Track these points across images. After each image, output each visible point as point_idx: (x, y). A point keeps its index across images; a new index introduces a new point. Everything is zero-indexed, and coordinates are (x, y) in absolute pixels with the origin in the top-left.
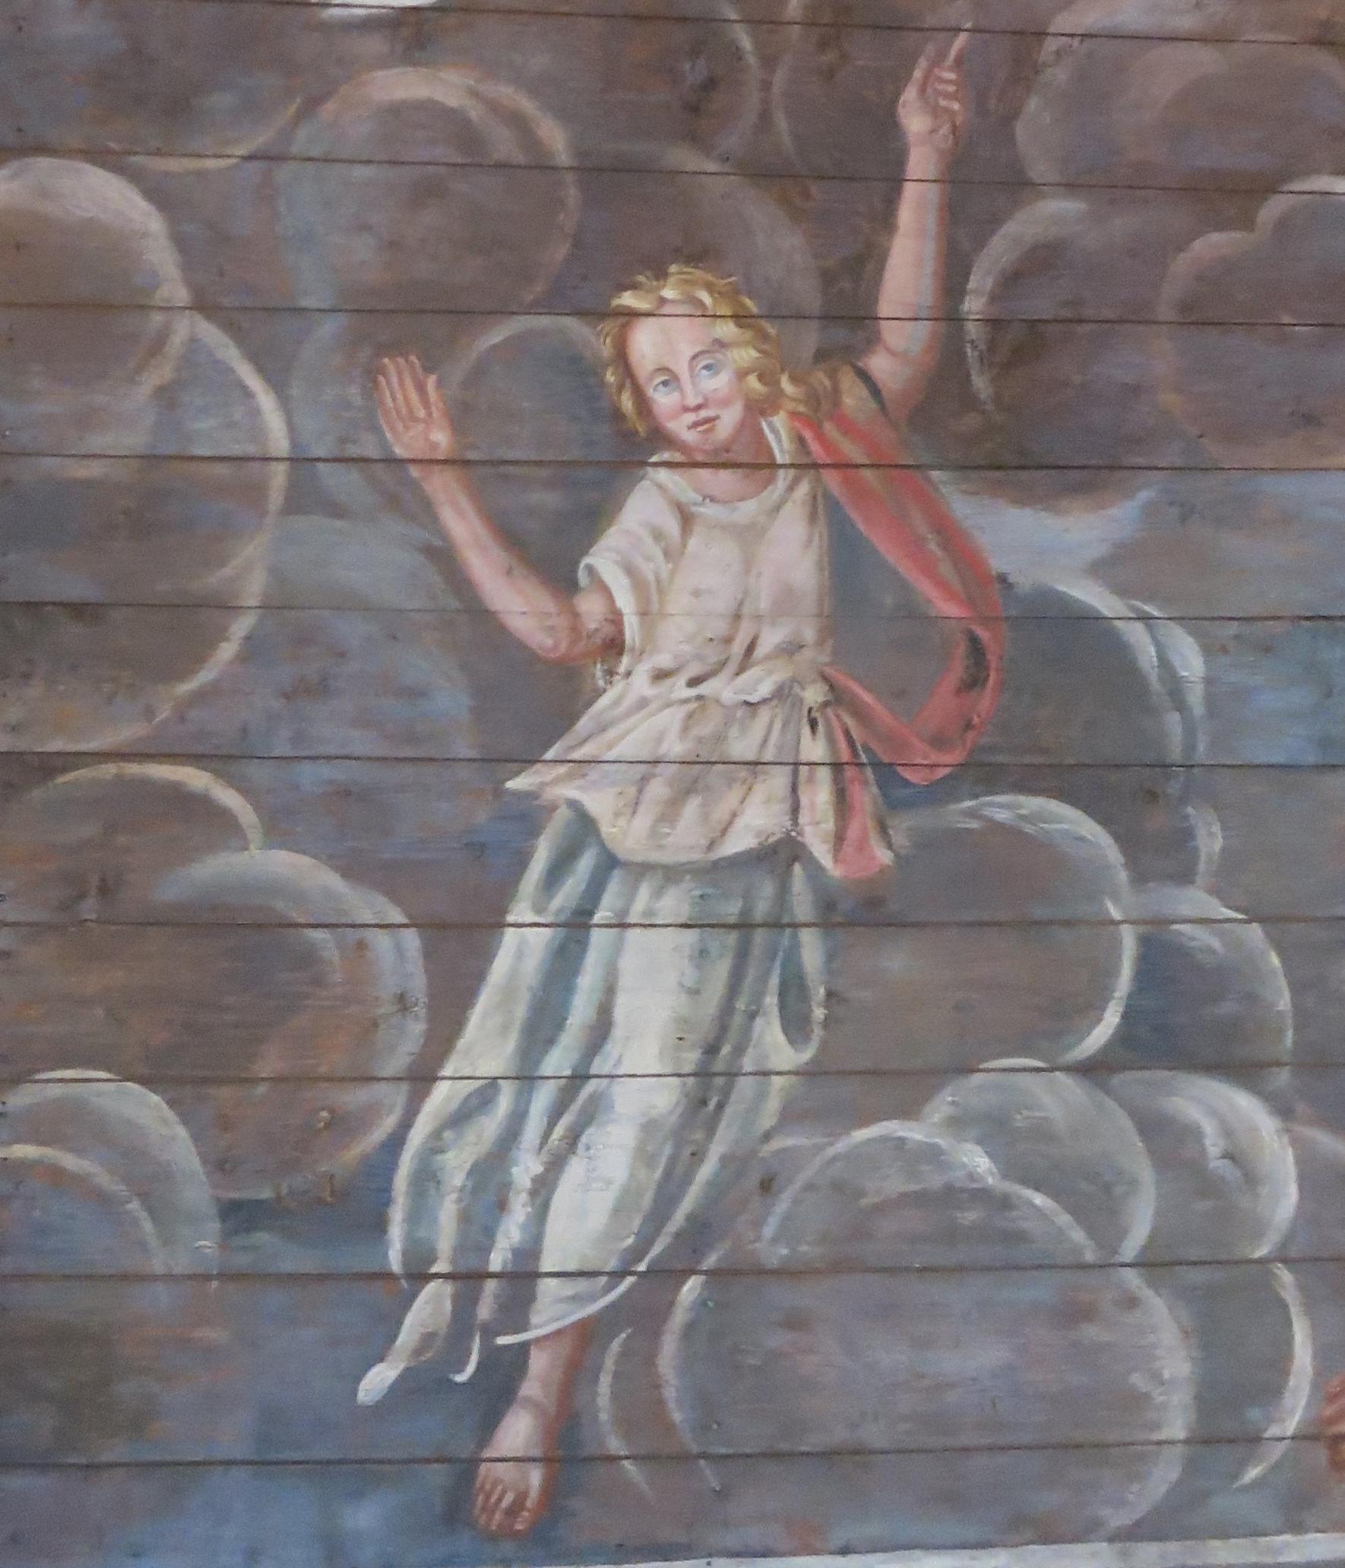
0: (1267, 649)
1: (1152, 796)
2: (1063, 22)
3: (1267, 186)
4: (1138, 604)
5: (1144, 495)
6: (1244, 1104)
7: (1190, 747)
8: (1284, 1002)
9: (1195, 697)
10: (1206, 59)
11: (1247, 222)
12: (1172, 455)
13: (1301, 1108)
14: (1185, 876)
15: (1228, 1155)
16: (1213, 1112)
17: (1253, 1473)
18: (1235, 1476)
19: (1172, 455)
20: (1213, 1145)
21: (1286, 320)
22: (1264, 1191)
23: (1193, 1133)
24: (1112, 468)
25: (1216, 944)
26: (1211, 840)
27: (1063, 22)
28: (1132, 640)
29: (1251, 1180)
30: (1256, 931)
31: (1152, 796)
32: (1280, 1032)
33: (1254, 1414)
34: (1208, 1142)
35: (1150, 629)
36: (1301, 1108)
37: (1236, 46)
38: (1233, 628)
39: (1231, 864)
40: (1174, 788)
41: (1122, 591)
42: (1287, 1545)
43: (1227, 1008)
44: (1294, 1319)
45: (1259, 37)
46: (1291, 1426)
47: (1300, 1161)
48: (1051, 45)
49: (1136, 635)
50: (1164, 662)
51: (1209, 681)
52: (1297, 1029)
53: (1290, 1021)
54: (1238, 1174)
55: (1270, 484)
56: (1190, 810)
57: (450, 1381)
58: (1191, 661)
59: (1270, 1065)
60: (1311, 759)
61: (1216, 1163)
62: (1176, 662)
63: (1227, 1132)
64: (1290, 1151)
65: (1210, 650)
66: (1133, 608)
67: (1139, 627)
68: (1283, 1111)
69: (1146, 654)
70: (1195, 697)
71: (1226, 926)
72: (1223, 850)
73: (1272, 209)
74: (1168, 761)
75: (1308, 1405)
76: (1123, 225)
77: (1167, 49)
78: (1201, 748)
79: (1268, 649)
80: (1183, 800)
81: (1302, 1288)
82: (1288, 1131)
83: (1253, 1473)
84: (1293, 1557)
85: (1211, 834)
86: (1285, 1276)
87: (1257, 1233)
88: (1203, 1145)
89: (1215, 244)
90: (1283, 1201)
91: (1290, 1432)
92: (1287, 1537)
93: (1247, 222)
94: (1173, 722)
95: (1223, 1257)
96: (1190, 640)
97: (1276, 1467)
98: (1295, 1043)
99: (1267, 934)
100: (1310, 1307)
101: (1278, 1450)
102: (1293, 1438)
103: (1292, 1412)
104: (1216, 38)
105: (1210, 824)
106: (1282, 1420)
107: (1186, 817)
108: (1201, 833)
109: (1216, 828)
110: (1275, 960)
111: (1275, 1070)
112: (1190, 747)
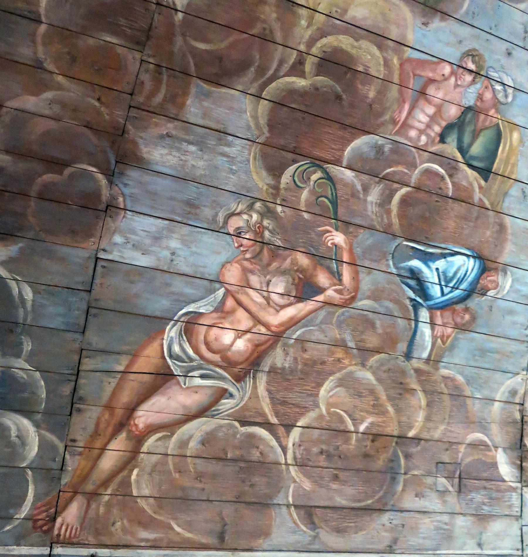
0: (52, 294)
1: (11, 331)
2: (9, 104)
3: (66, 164)
4: (15, 276)
5: (20, 245)
6: (26, 422)
7: (25, 319)
8: (44, 396)
9: (29, 305)
10: (52, 125)
11: (61, 174)
12: (30, 235)
13: (43, 425)
14: (18, 356)
15: (17, 436)
16: (16, 424)
17: (8, 528)
18: (3, 527)
19: (30, 235)
20: (14, 433)
21: (70, 203)
22: (27, 448)
23: (9, 429)
24: (12, 235)
25: (25, 376)
26: (28, 346)
27: (9, 104)
28: (11, 286)
29: (24, 444)
30: (38, 374)
31: (11, 331)
32: (41, 403)
33: (11, 511)
34: (12, 432)
35: (17, 284)
36: (43, 425)
37: (61, 122)
38: (43, 287)
39: (32, 353)
40: (19, 330)
41: (10, 271)
42: (14, 549)
43: (26, 395)
44: (30, 485)
45: (68, 121)
46: (22, 516)
47: (39, 441)
48: (4, 110)
49: (13, 284)
50: (20, 292)
51: (33, 301)
52: (46, 404)
53: (44, 400)
54: (20, 442)
55: (59, 248)
56: (23, 337)
57: (136, 468)
58: (29, 294)
59: (34, 412)
60: (62, 328)
61: (13, 438)
62: (24, 293)
63: (19, 430)
64: (37, 437)
65: (35, 292)
66: (13, 277)
67: (14, 282)
68: (37, 425)
69: (15, 291)
70: (29, 305)
71: (28, 371)
72: (31, 349)
73: (68, 171)
74: (18, 322)
75: (30, 509)
76: (23, 166)
77: (40, 119)
78: (29, 320)
79: (53, 295)
80: (21, 334)
81: (33, 477)
82: (38, 431)
83: (8, 528)
84: (16, 553)
85: (28, 345)
86: (30, 473)
87: (24, 459)
88: (10, 433)
89: (48, 177)
90: (33, 450)
91: (22, 517)
92: (15, 547)
93: (61, 174)
94: (21, 311)
95: (11, 465)
96: (30, 288)
97: (15, 527)
98: (45, 407)
99: (41, 375)
100: (35, 483)
101: (17, 522)
102: (23, 519)
103: (24, 512)
104: (56, 119)
105: (28, 342)
106: (20, 514)
107: (21, 339)
108: (25, 343)
109: (30, 344)
110: (43, 383)
111: (37, 414)
112: (25, 319)
